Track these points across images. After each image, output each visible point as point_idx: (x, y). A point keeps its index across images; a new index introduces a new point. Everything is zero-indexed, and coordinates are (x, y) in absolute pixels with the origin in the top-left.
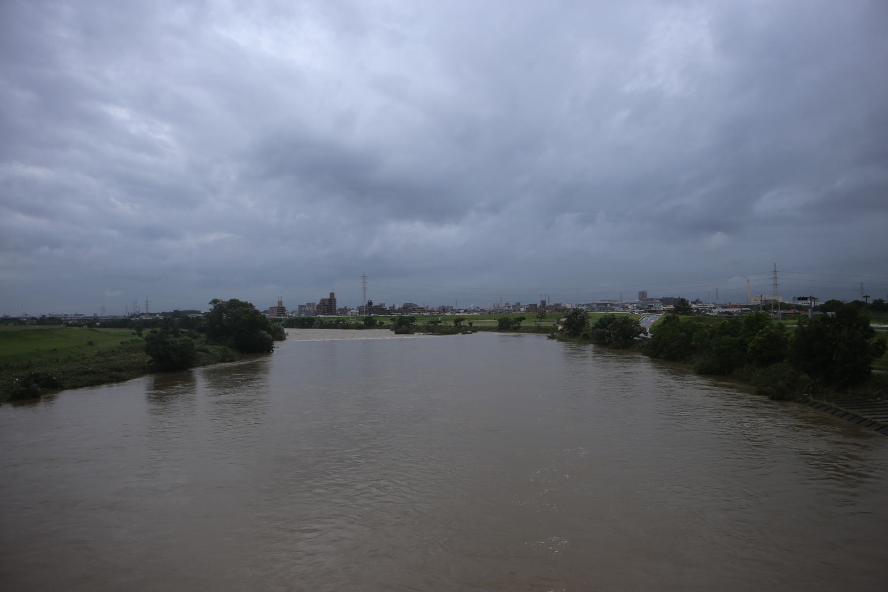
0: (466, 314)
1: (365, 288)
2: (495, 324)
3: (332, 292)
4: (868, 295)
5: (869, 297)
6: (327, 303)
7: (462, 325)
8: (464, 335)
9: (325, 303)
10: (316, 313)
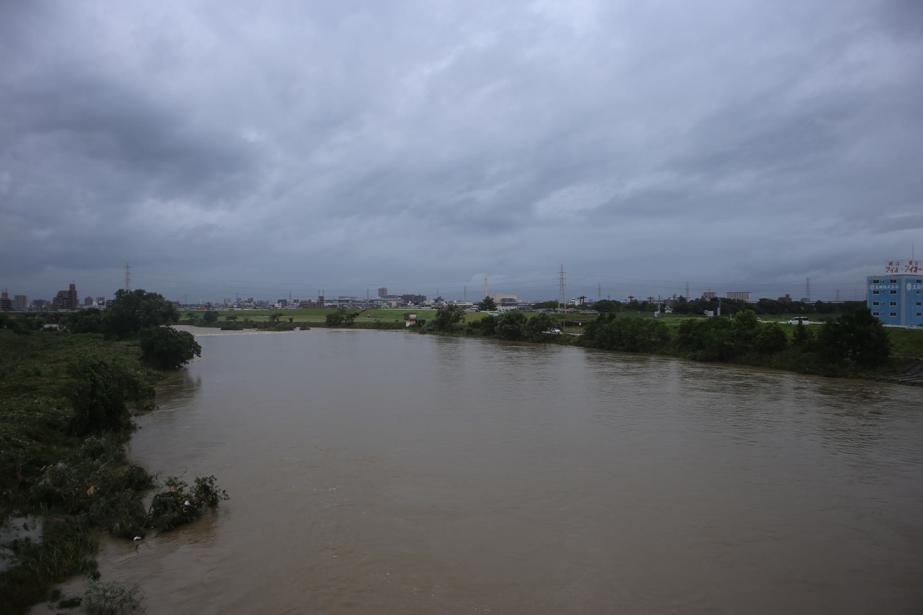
0: (240, 309)
2: (323, 320)
3: (72, 283)
4: (632, 296)
5: (633, 297)
6: (66, 296)
7: (280, 320)
8: (303, 331)
10: (54, 307)
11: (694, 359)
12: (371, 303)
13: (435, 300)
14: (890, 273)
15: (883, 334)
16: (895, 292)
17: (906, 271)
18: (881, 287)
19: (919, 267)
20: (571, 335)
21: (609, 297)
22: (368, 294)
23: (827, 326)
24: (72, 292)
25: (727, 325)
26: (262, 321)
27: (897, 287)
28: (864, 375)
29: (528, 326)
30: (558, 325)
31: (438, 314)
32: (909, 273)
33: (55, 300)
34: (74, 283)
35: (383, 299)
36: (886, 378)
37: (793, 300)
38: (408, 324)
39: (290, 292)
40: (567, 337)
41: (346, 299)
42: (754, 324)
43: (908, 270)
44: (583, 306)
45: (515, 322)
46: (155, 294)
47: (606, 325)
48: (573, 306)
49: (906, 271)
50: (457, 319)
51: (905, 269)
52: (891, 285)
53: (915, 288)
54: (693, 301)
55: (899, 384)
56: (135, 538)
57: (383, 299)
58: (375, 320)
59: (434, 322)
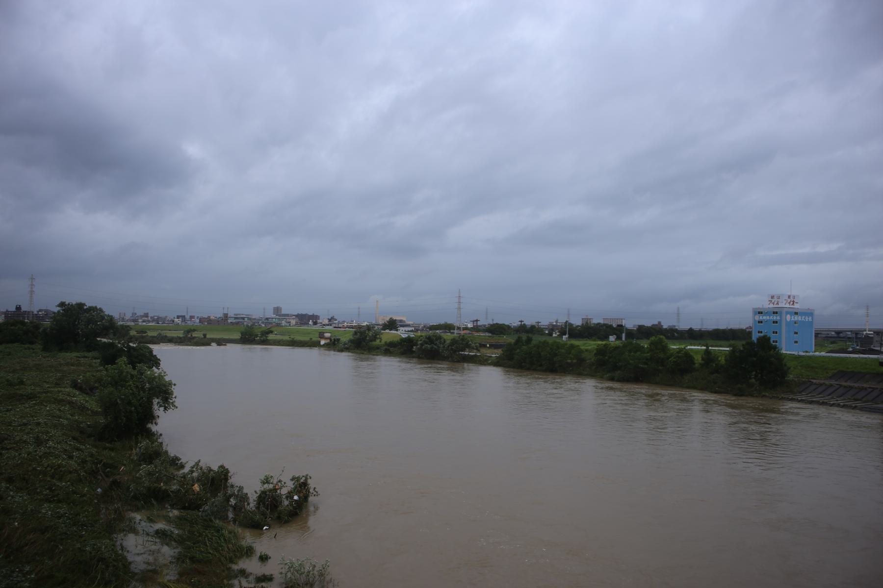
0: (144, 324)
1: (32, 292)
2: (237, 336)
4: (540, 321)
7: (193, 336)
11: (612, 379)
12: (266, 321)
13: (328, 319)
14: (771, 306)
15: (780, 357)
16: (777, 322)
17: (785, 304)
18: (764, 318)
19: (796, 301)
20: (488, 356)
21: (493, 320)
23: (733, 352)
25: (639, 349)
26: (175, 335)
27: (778, 318)
28: (767, 394)
29: (449, 346)
30: (476, 346)
31: (355, 333)
32: (787, 306)
35: (277, 317)
36: (786, 396)
37: (665, 327)
38: (323, 342)
39: (187, 308)
40: (485, 358)
41: (242, 316)
42: (664, 349)
43: (787, 304)
44: (476, 329)
45: (435, 343)
46: (96, 307)
47: (524, 347)
48: (466, 328)
49: (785, 304)
50: (374, 338)
51: (785, 302)
52: (773, 316)
53: (793, 319)
54: (579, 326)
55: (799, 402)
56: (265, 528)
57: (277, 317)
58: (290, 338)
59: (351, 341)
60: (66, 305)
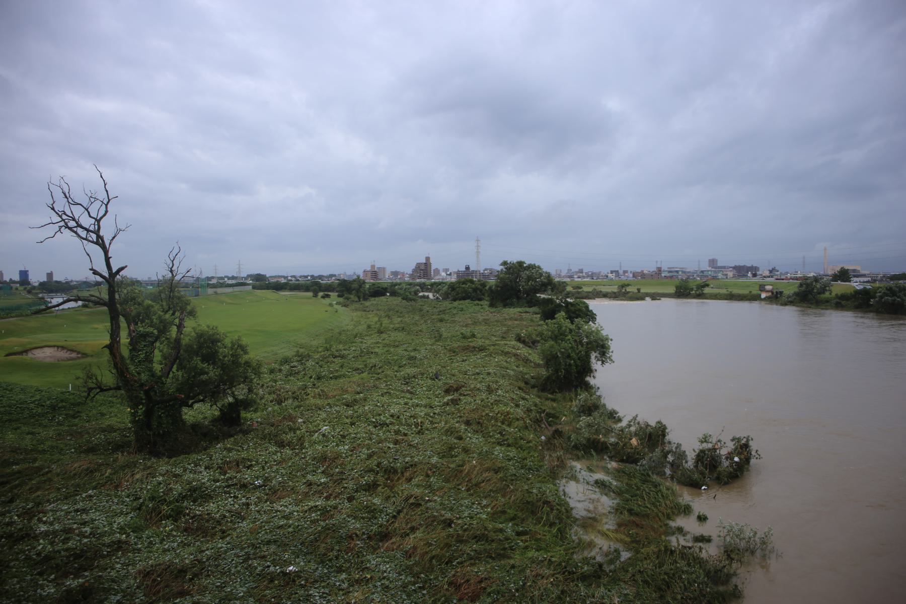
0: (580, 280)
2: (672, 290)
5: (637, 416)
6: (423, 267)
7: (628, 290)
9: (421, 268)
13: (769, 270)
22: (699, 265)
24: (427, 264)
26: (610, 291)
31: (801, 285)
33: (414, 271)
34: (708, 260)
35: (713, 269)
38: (763, 295)
56: (703, 488)
57: (713, 269)
59: (796, 294)
60: (508, 264)
